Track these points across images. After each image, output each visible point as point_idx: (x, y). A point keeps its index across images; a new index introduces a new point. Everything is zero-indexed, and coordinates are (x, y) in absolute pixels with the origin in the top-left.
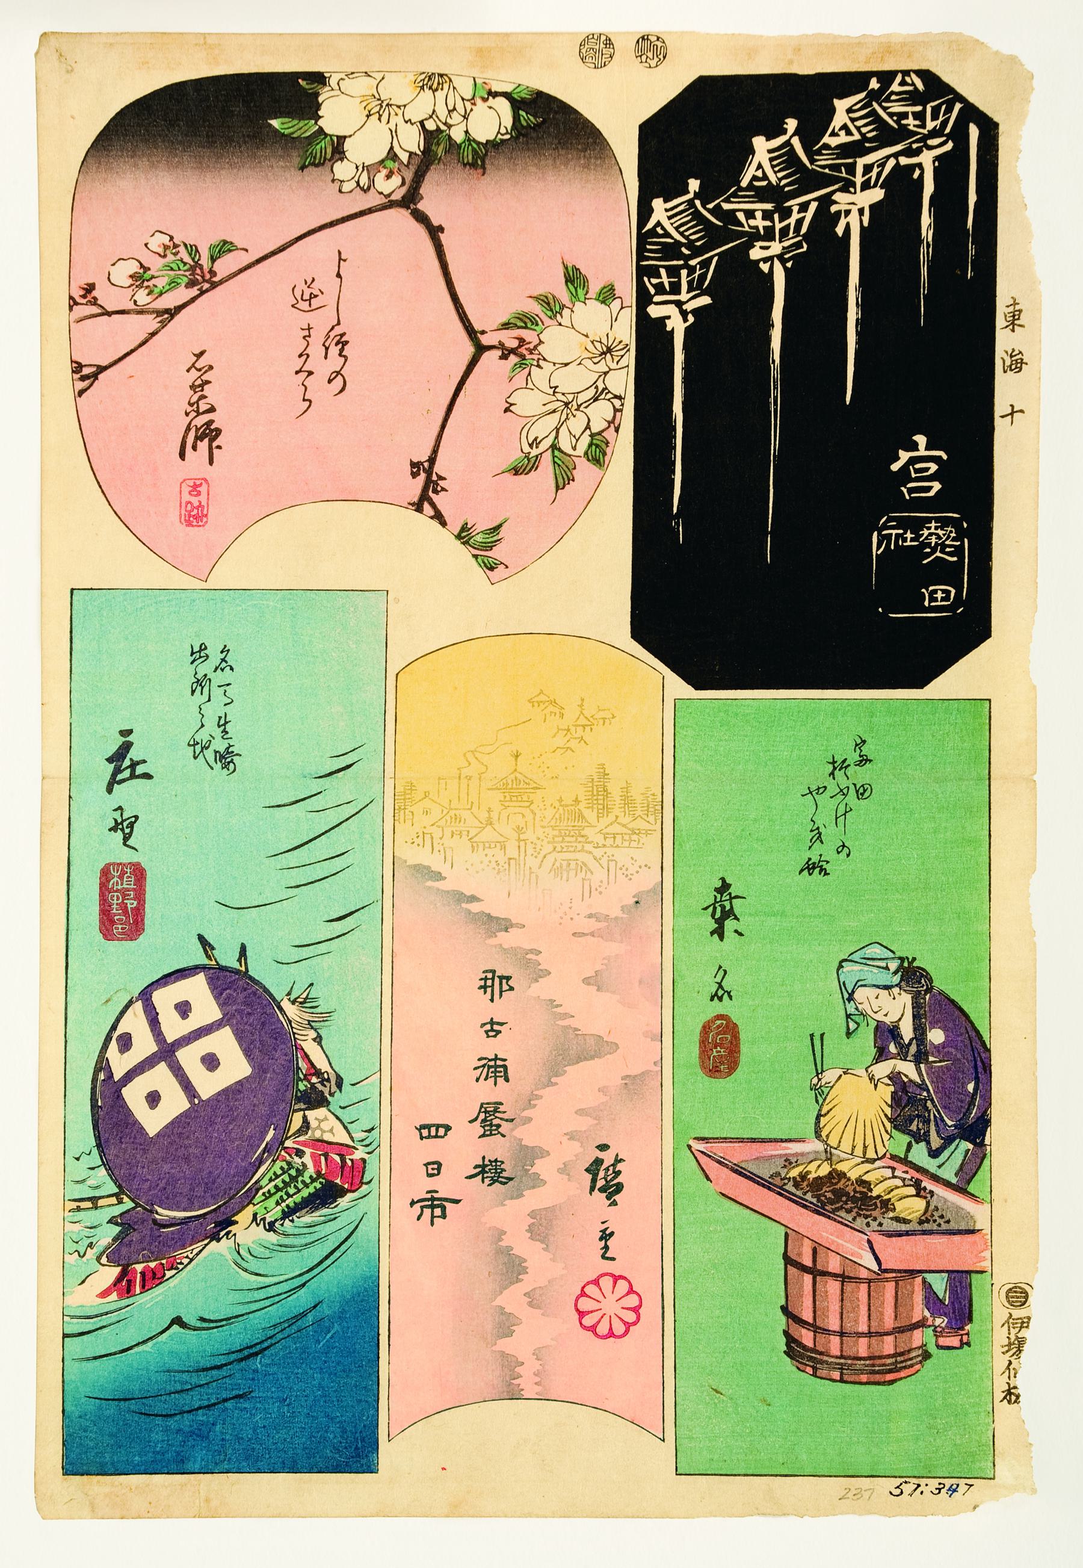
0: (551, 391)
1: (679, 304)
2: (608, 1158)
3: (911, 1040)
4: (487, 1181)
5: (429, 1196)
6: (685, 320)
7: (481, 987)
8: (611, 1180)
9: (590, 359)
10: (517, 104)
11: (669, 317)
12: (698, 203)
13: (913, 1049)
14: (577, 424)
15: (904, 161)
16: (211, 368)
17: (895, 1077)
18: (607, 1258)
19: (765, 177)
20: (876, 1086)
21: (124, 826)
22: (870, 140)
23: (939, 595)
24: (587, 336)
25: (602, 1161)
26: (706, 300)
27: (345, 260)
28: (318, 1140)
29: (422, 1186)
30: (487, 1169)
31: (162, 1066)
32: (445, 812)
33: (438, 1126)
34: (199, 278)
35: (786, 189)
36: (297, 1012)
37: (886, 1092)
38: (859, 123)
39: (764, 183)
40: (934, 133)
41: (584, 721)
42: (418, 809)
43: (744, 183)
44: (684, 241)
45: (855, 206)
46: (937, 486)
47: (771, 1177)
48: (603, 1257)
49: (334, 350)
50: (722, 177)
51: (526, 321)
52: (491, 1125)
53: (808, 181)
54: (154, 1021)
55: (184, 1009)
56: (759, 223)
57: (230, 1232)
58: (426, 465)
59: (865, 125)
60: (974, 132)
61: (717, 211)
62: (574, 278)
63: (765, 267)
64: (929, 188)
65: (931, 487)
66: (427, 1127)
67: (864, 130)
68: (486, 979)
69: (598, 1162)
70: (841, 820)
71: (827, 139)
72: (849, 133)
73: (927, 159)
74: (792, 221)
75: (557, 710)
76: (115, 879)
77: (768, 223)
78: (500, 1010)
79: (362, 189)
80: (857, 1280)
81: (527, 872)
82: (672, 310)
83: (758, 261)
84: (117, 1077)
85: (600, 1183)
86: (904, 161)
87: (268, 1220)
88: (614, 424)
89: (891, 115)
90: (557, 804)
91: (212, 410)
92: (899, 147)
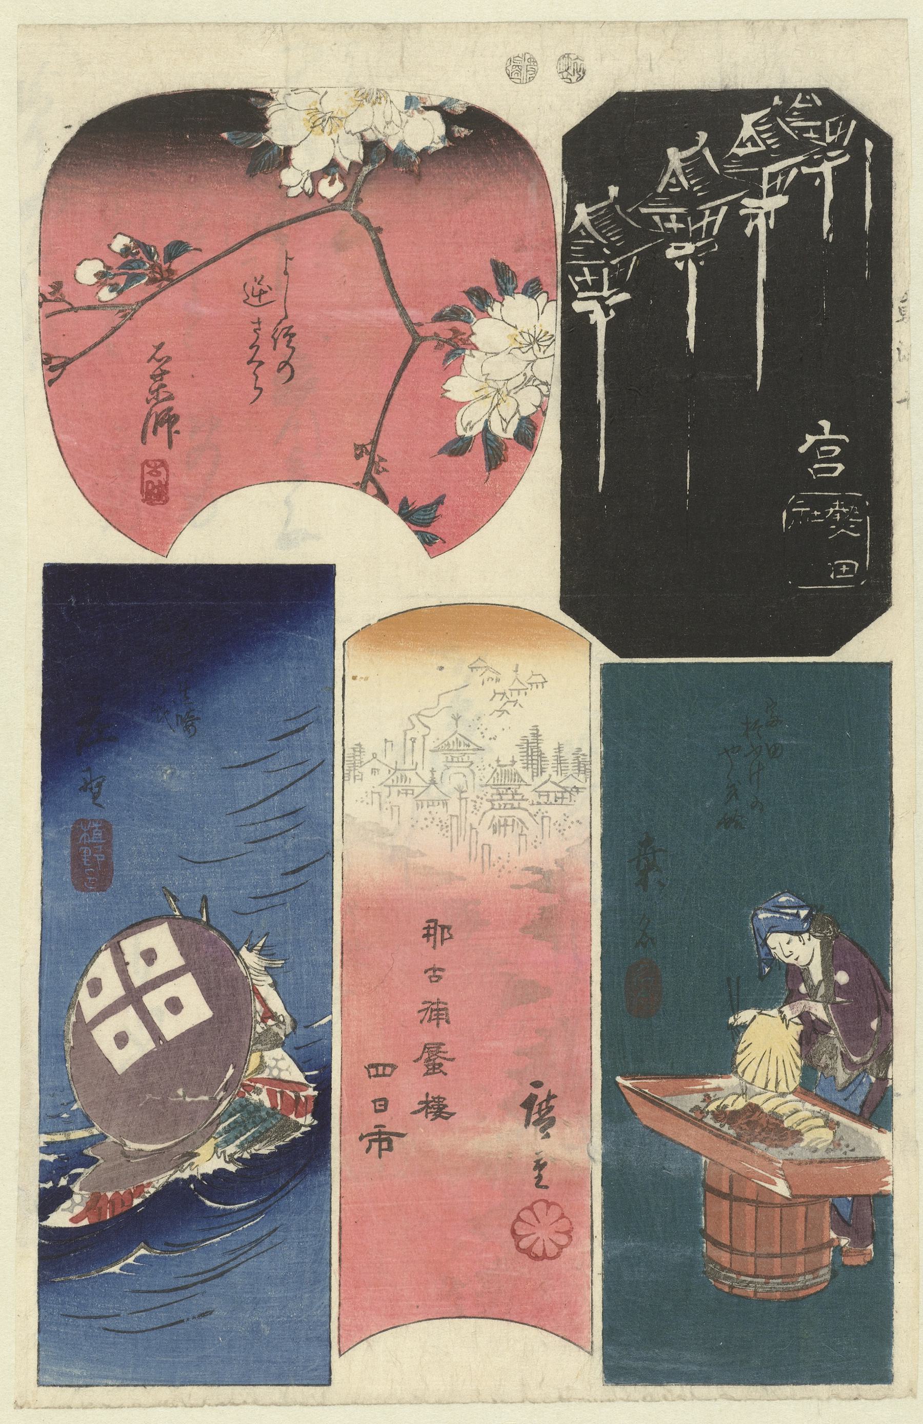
0: (483, 379)
1: (601, 300)
2: (542, 1094)
3: (820, 982)
4: (430, 1116)
5: (377, 1130)
6: (607, 314)
7: (424, 936)
8: (544, 1115)
9: (519, 348)
10: (449, 118)
11: (592, 312)
12: (618, 207)
13: (822, 991)
14: (507, 409)
15: (805, 170)
16: (169, 358)
17: (804, 1017)
18: (541, 1187)
19: (679, 184)
20: (787, 1026)
21: (435, 974)
22: (775, 151)
23: (844, 568)
24: (516, 327)
25: (536, 1096)
26: (624, 296)
27: (291, 259)
28: (275, 1079)
29: (372, 1121)
30: (430, 1105)
31: (130, 1011)
32: (392, 771)
33: (385, 1066)
34: (158, 276)
35: (699, 194)
36: (256, 960)
37: (796, 1029)
38: (765, 136)
39: (678, 189)
40: (833, 146)
41: (517, 685)
42: (366, 770)
43: (660, 189)
44: (605, 242)
45: (764, 209)
46: (840, 467)
47: (691, 1110)
48: (537, 1185)
49: (282, 343)
50: (641, 187)
51: (456, 313)
52: (434, 1065)
53: (717, 186)
54: (122, 967)
55: (149, 956)
56: (674, 225)
57: (193, 1163)
58: (369, 447)
59: (769, 138)
60: (869, 145)
61: (636, 215)
62: (501, 272)
63: (680, 266)
64: (829, 195)
65: (836, 468)
66: (375, 1066)
67: (769, 142)
68: (428, 928)
69: (532, 1099)
70: (755, 778)
71: (734, 150)
72: (755, 144)
73: (826, 168)
74: (704, 223)
75: (494, 676)
76: (84, 835)
77: (682, 226)
78: (444, 954)
79: (307, 194)
80: (773, 1205)
81: (468, 828)
82: (594, 306)
83: (674, 260)
84: (88, 1020)
85: (535, 1117)
86: (805, 170)
87: (228, 1153)
88: (542, 410)
89: (793, 129)
90: (495, 765)
91: (170, 397)
92: (800, 158)
